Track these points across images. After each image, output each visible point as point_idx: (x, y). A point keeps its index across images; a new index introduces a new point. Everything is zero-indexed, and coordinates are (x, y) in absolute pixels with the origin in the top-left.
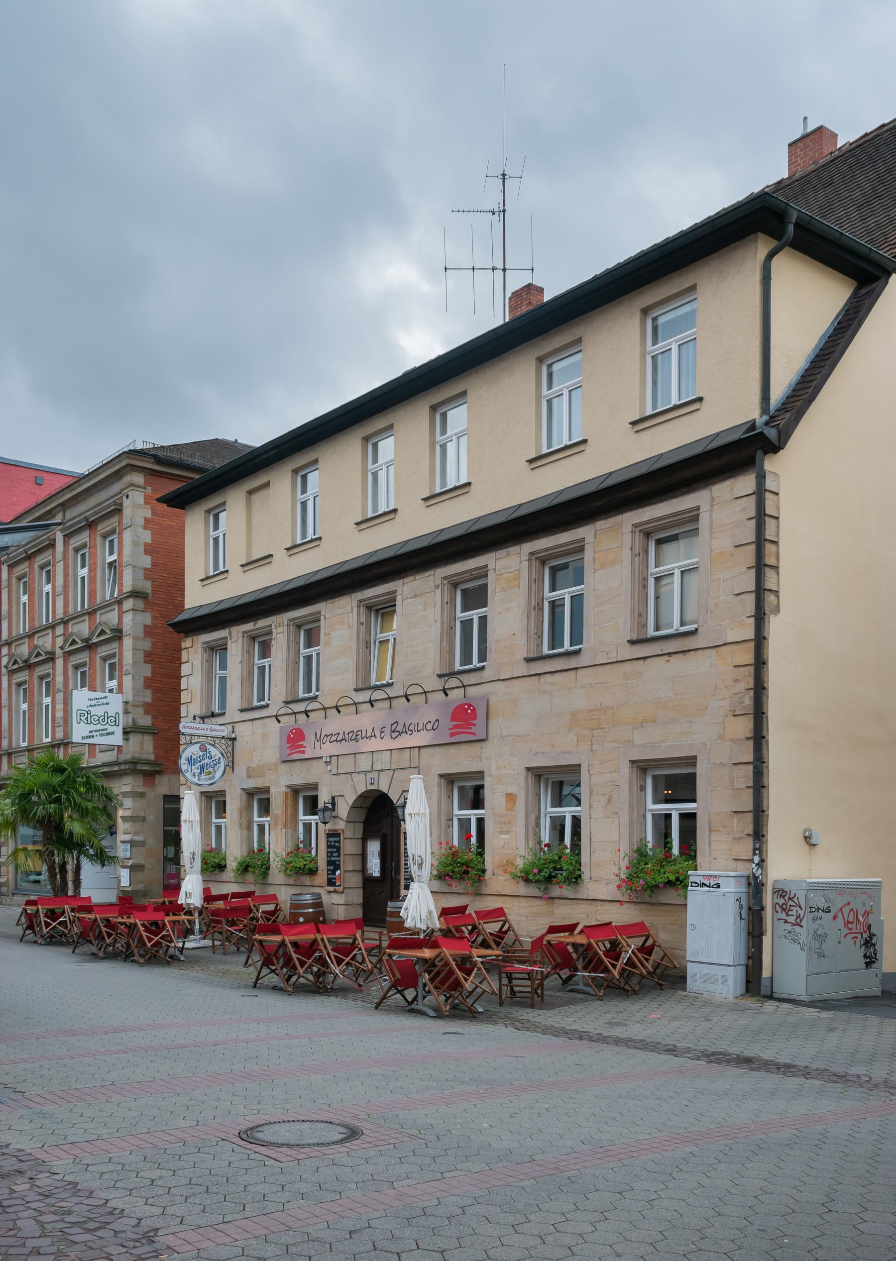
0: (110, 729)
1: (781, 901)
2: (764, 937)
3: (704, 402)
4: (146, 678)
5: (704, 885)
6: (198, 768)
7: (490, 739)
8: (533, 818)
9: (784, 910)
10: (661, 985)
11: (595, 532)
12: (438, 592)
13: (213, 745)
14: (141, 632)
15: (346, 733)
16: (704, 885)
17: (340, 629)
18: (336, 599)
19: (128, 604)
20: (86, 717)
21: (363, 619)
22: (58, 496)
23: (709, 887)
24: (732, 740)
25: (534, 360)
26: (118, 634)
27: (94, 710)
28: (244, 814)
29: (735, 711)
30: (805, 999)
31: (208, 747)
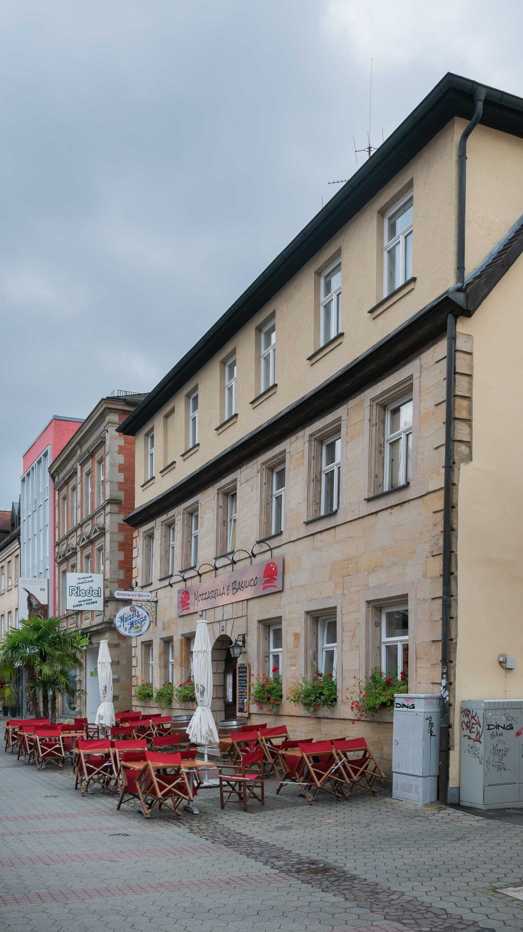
0: (94, 599)
1: (466, 720)
2: (451, 752)
3: (417, 281)
4: (120, 562)
5: (404, 706)
6: (128, 624)
7: (285, 590)
8: (310, 653)
9: (468, 727)
10: (374, 792)
11: (348, 410)
12: (259, 475)
13: (141, 607)
14: (116, 529)
15: (210, 592)
16: (404, 706)
17: (208, 513)
18: (207, 490)
19: (108, 509)
20: (76, 591)
21: (221, 504)
22: (75, 437)
23: (407, 707)
24: (431, 578)
25: (313, 274)
26: (103, 531)
27: (82, 586)
28: (162, 656)
29: (433, 552)
30: (482, 807)
31: (137, 608)
